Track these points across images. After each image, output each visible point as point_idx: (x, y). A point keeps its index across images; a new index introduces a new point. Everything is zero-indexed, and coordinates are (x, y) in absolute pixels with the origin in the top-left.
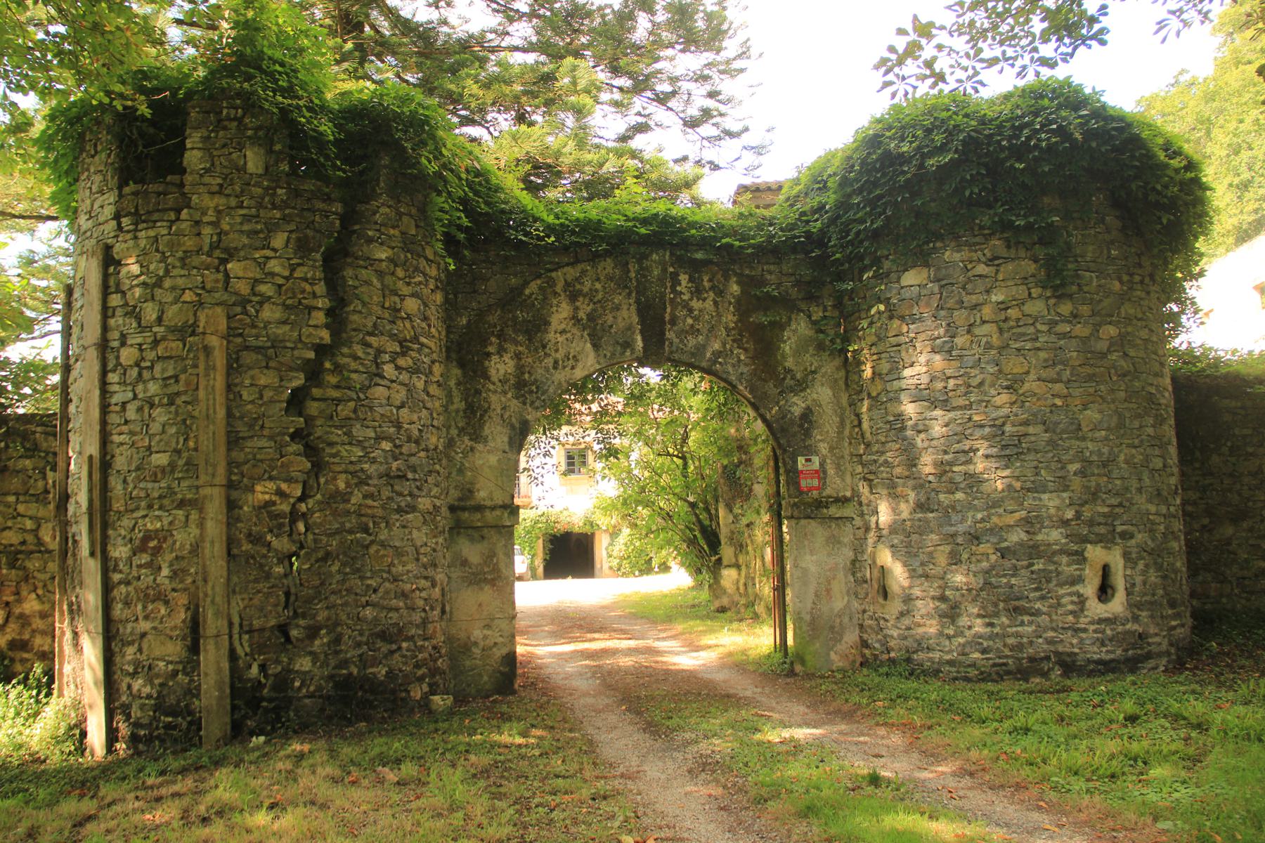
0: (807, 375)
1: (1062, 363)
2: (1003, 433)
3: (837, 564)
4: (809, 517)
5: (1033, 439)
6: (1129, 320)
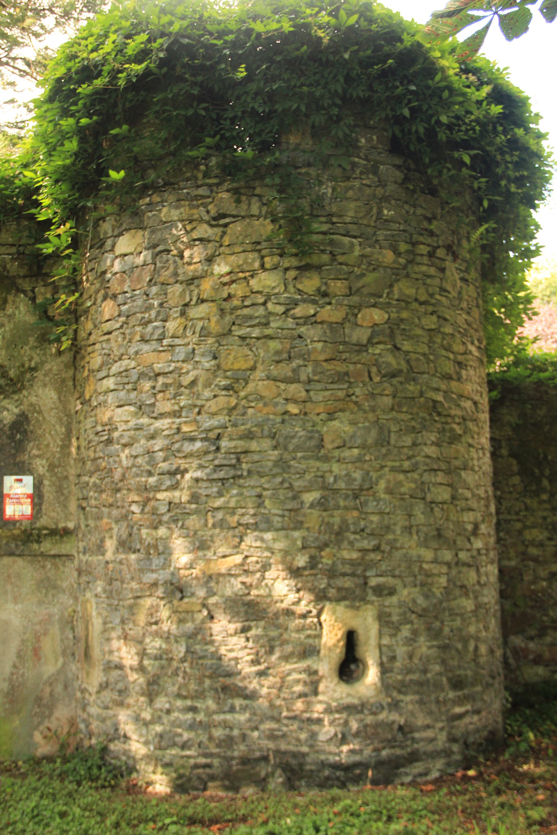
0: (23, 373)
1: (301, 356)
2: (218, 449)
3: (50, 616)
4: (12, 554)
5: (256, 457)
6: (404, 302)
